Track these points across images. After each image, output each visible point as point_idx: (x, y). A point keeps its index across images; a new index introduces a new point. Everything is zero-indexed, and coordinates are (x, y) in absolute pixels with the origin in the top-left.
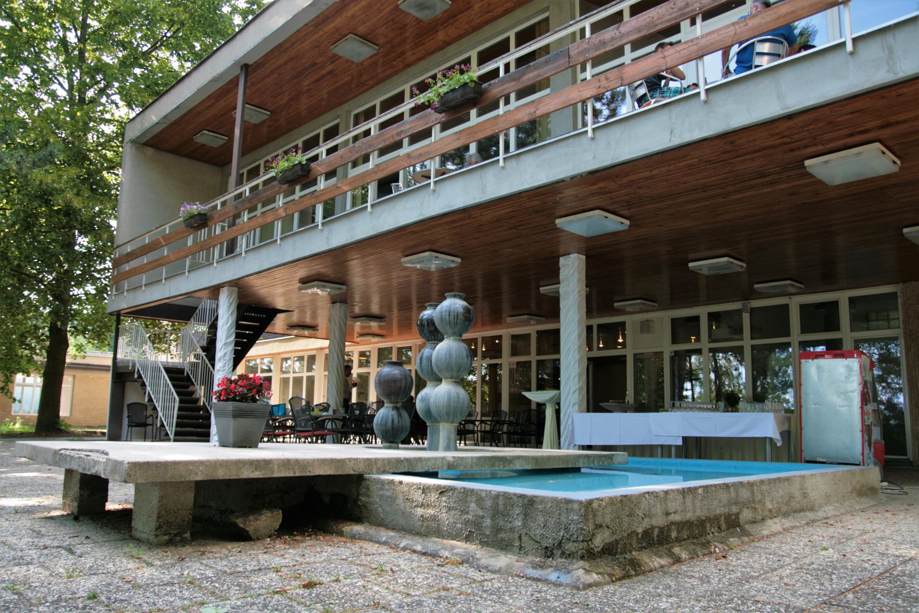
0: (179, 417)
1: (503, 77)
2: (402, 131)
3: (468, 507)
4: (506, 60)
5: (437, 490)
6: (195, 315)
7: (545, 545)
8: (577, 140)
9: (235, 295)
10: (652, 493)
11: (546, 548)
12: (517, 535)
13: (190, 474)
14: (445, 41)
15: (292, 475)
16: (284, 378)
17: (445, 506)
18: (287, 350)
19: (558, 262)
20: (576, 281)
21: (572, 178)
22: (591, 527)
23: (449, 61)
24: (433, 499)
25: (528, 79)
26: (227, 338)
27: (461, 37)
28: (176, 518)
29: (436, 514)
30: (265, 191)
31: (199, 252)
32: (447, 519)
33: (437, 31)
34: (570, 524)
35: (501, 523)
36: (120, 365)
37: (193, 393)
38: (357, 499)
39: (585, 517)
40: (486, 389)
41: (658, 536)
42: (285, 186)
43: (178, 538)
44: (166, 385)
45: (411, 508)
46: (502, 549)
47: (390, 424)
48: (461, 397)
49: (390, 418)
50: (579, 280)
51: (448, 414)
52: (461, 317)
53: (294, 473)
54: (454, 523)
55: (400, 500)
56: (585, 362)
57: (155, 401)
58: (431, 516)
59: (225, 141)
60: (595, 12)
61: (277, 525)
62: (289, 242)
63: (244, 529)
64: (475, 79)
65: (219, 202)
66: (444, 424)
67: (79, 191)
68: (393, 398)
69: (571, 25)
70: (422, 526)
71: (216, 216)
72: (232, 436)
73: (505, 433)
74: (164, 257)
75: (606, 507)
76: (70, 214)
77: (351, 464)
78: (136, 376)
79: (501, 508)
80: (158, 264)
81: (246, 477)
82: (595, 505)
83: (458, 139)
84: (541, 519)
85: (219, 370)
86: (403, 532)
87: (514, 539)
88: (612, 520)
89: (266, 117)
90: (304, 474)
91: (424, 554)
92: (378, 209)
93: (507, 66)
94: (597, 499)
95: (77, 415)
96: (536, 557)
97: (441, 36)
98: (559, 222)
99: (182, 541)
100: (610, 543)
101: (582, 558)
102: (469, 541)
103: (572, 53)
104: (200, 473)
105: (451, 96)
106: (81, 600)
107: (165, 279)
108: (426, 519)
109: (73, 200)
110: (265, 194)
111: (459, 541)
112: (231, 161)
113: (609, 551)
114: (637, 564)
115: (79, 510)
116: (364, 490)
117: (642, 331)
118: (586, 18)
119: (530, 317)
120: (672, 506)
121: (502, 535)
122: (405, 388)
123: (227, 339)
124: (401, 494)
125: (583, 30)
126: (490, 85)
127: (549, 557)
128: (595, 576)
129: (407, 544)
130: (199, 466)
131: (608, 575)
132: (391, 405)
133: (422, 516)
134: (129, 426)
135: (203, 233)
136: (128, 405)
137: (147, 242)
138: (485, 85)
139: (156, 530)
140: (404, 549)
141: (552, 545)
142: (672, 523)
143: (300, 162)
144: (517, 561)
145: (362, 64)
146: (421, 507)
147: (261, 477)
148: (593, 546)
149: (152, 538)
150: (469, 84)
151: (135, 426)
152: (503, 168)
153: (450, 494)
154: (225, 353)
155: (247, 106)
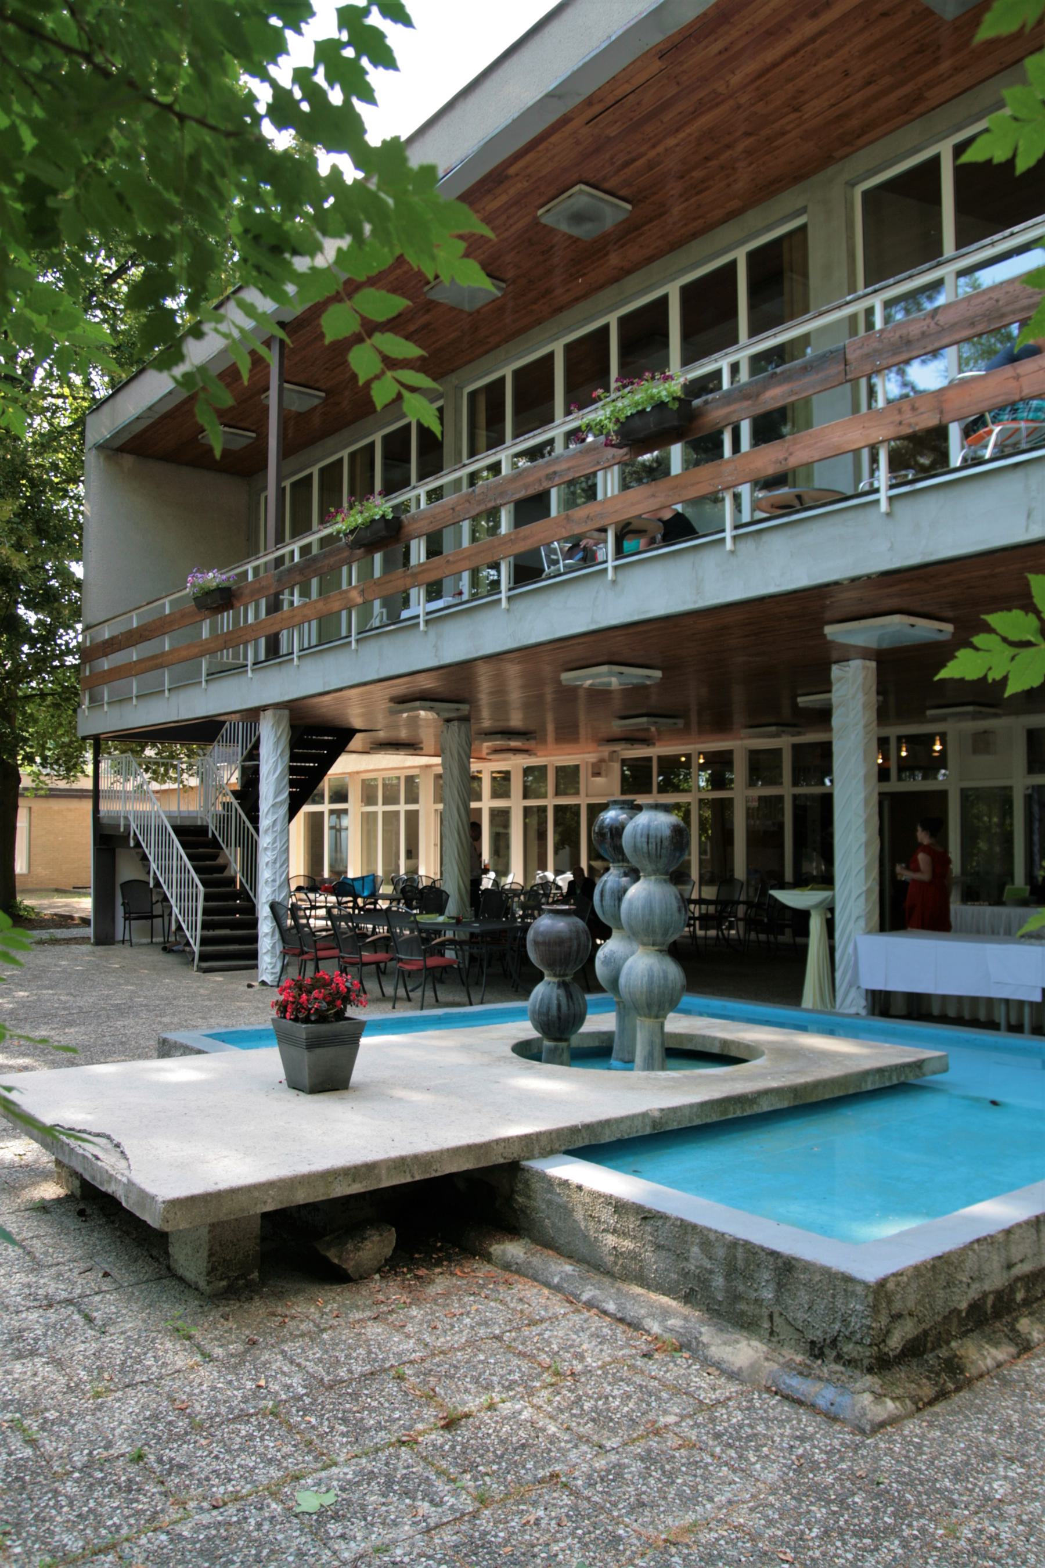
0: (206, 912)
1: (728, 391)
2: (555, 473)
3: (689, 1251)
4: (732, 359)
5: (638, 1213)
6: (219, 736)
7: (811, 1337)
8: (861, 514)
9: (285, 724)
10: (985, 1239)
11: (813, 1343)
12: (765, 1312)
13: (256, 1204)
14: (622, 269)
15: (409, 1180)
16: (369, 813)
17: (651, 1241)
18: (371, 767)
19: (829, 670)
20: (860, 707)
21: (853, 580)
22: (884, 1320)
23: (629, 302)
24: (631, 1226)
25: (773, 398)
26: (276, 796)
27: (650, 260)
28: (237, 1253)
29: (637, 1250)
30: (325, 556)
31: (222, 650)
32: (655, 1262)
33: (607, 254)
34: (851, 1315)
35: (741, 1288)
36: (104, 821)
37: (223, 868)
38: (509, 1199)
39: (875, 1309)
40: (708, 813)
41: (993, 1306)
42: (359, 552)
43: (241, 1282)
44: (182, 869)
45: (596, 1231)
46: (742, 1327)
47: (554, 1011)
48: (671, 977)
49: (555, 1002)
50: (865, 706)
51: (649, 1006)
52: (666, 843)
53: (413, 1177)
54: (666, 1270)
55: (579, 1215)
56: (875, 799)
57: (144, 845)
58: (630, 1252)
59: (250, 441)
60: (891, 281)
61: (388, 1251)
62: (372, 649)
63: (339, 1267)
64: (679, 393)
65: (249, 568)
66: (643, 1019)
67: (20, 538)
68: (558, 969)
69: (847, 303)
70: (616, 1263)
71: (247, 591)
72: (307, 1076)
73: (740, 920)
74: (163, 654)
75: (908, 1284)
76: (9, 580)
77: (500, 1149)
78: (132, 844)
79: (740, 1264)
80: (155, 663)
81: (339, 1195)
82: (891, 1286)
83: (653, 496)
84: (804, 1297)
85: (266, 849)
86: (586, 1266)
87: (761, 1317)
88: (919, 1302)
89: (316, 402)
90: (427, 1176)
91: (621, 1320)
92: (520, 606)
93: (735, 368)
94: (894, 1275)
95: (40, 871)
96: (797, 1352)
97: (614, 259)
98: (828, 630)
99: (247, 1286)
100: (916, 1339)
101: (870, 1370)
102: (690, 1302)
103: (851, 356)
104: (270, 1201)
105: (638, 422)
106: (120, 1462)
107: (169, 690)
108: (621, 1254)
109: (12, 558)
110: (327, 562)
111: (674, 1299)
112: (266, 467)
113: (914, 1350)
114: (958, 1368)
115: (82, 1192)
116: (520, 1186)
117: (976, 751)
118: (875, 291)
119: (781, 728)
120: (1016, 1253)
121: (742, 1306)
122: (578, 952)
123: (276, 797)
124: (580, 1206)
125: (870, 312)
126: (706, 402)
127: (817, 1357)
128: (890, 1404)
129: (594, 1297)
130: (268, 1191)
131: (911, 1398)
132: (556, 980)
133: (614, 1248)
134: (126, 919)
135: (226, 620)
136: (124, 885)
137: (135, 625)
138: (697, 402)
139: (209, 1274)
140: (589, 1305)
141: (821, 1340)
142: (1018, 1279)
143: (383, 516)
144: (767, 1359)
145: (478, 312)
146: (613, 1233)
147: (363, 1190)
148: (887, 1349)
149: (202, 1284)
150: (670, 405)
151: (135, 919)
152: (732, 552)
153: (660, 1223)
154: (275, 821)
155: (286, 385)
